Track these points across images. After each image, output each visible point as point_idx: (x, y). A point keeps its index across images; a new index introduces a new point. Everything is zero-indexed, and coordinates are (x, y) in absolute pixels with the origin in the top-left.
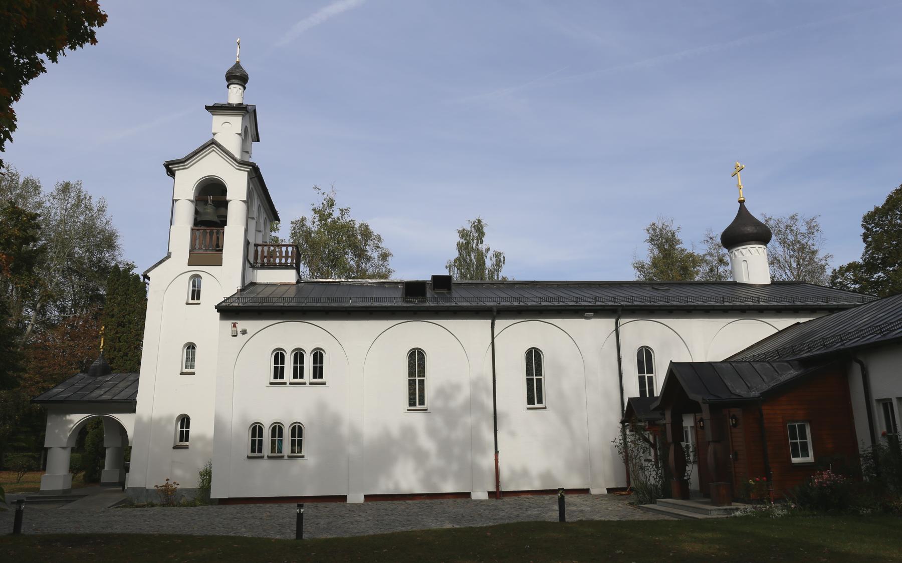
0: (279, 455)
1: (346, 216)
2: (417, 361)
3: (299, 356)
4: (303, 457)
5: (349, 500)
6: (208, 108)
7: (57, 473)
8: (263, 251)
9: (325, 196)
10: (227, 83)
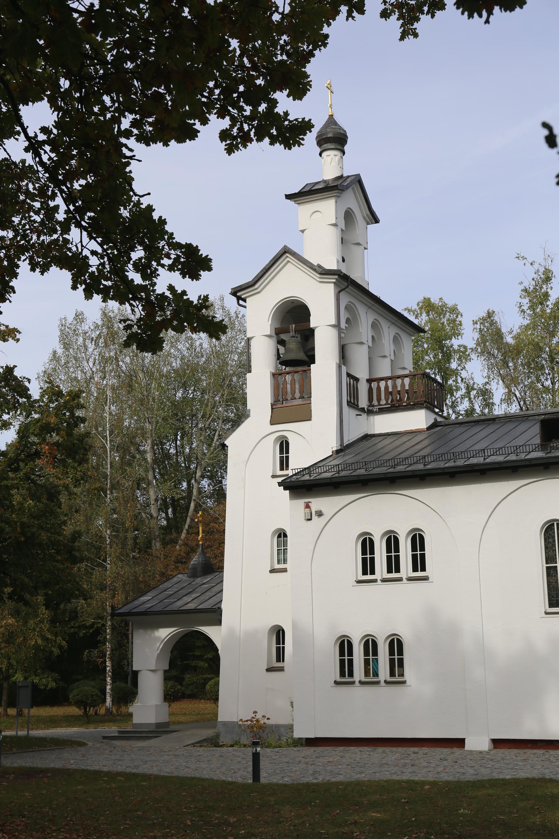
0: (375, 680)
3: (392, 542)
5: (469, 746)
6: (288, 197)
7: (149, 704)
9: (536, 266)
10: (318, 150)
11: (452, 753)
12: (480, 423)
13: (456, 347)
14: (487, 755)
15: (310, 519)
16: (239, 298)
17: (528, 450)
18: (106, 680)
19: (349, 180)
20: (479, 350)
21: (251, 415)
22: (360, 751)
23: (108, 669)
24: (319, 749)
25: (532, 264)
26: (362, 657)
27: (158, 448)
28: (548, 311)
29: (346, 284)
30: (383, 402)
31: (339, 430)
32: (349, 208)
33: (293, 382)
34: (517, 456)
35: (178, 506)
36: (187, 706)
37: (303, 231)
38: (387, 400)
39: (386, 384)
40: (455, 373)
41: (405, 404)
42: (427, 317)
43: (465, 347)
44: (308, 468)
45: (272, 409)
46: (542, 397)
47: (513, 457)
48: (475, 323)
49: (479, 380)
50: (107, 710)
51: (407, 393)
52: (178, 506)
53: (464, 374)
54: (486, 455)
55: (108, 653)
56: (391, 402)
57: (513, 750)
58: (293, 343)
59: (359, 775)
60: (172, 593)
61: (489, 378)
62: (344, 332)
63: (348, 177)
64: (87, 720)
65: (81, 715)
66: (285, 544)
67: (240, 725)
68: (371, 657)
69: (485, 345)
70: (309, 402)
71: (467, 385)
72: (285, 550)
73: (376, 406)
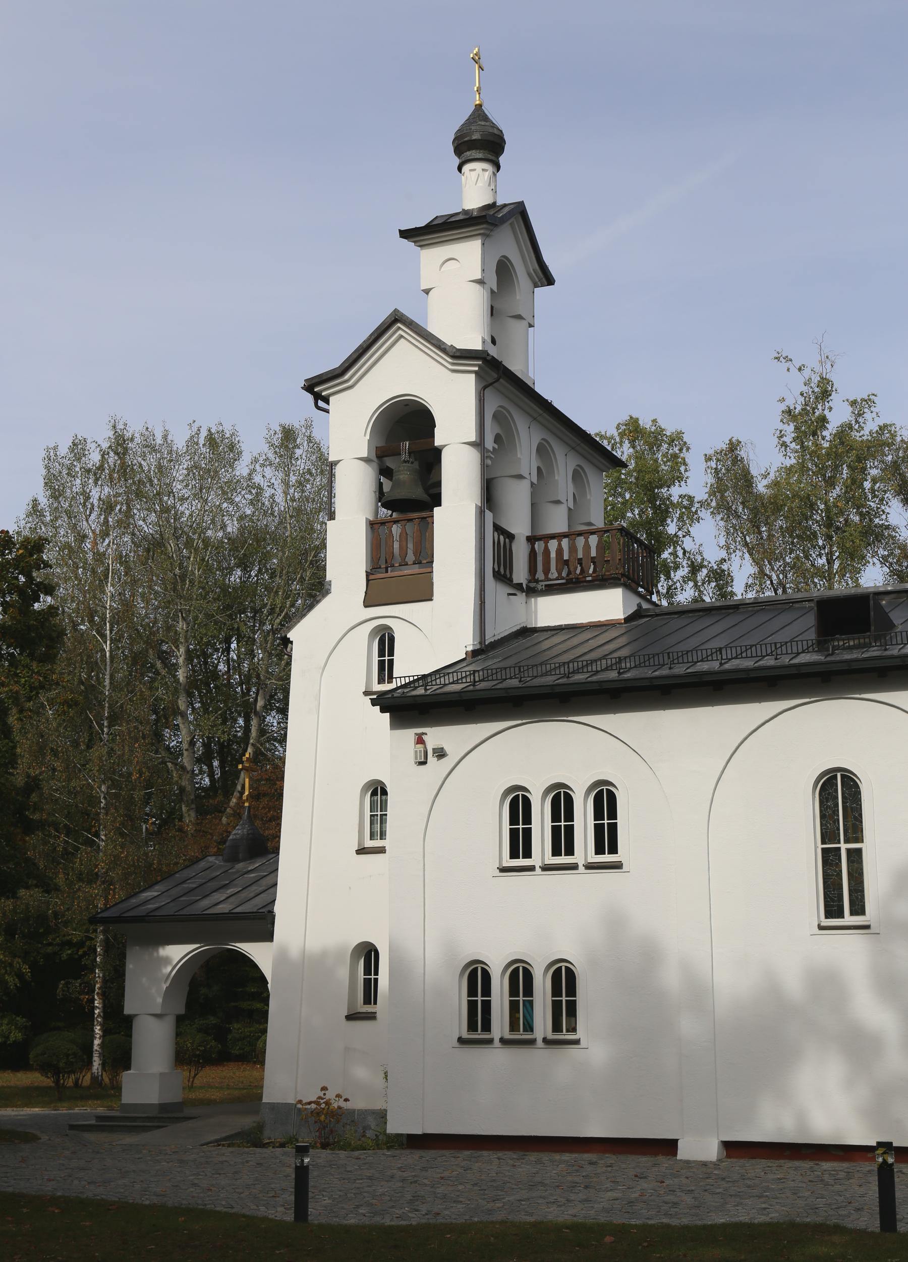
0: (485, 1036)
1: (868, 416)
2: (839, 800)
4: (577, 1042)
5: (684, 1152)
6: (406, 234)
7: (152, 1070)
8: (560, 551)
9: (807, 373)
10: (457, 161)
11: (655, 1165)
12: (713, 612)
13: (675, 499)
14: (715, 1169)
15: (424, 763)
16: (317, 397)
17: (795, 650)
18: (93, 1031)
19: (506, 210)
20: (714, 504)
21: (333, 589)
22: (499, 1159)
23: (97, 1011)
24: (429, 1154)
25: (800, 369)
26: (507, 999)
27: (199, 663)
28: (826, 445)
29: (495, 374)
30: (554, 573)
31: (478, 617)
32: (504, 257)
33: (404, 537)
34: (776, 659)
35: (225, 752)
36: (231, 1074)
37: (427, 292)
38: (559, 572)
39: (560, 545)
40: (674, 541)
41: (589, 578)
42: (631, 450)
43: (691, 499)
44: (424, 677)
45: (368, 580)
46: (814, 582)
47: (769, 662)
48: (708, 459)
49: (713, 555)
50: (94, 1078)
51: (594, 563)
52: (225, 752)
53: (688, 544)
54: (724, 657)
55: (98, 986)
56: (568, 575)
57: (758, 1161)
58: (405, 473)
59: (492, 1204)
60: (194, 886)
61: (728, 548)
62: (491, 458)
63: (505, 205)
64: (58, 1094)
65: (50, 1087)
66: (384, 807)
67: (299, 1109)
68: (521, 998)
69: (722, 496)
70: (429, 570)
71: (692, 562)
72: (383, 817)
73: (542, 581)
